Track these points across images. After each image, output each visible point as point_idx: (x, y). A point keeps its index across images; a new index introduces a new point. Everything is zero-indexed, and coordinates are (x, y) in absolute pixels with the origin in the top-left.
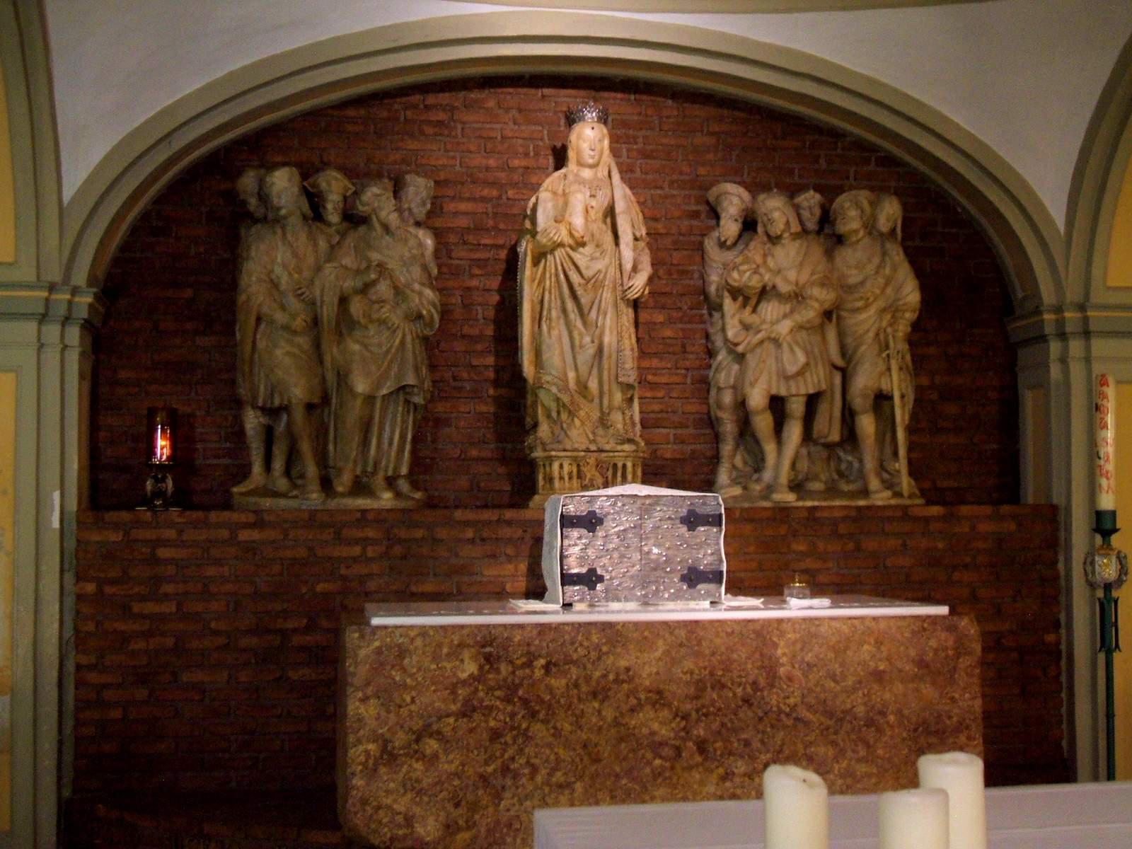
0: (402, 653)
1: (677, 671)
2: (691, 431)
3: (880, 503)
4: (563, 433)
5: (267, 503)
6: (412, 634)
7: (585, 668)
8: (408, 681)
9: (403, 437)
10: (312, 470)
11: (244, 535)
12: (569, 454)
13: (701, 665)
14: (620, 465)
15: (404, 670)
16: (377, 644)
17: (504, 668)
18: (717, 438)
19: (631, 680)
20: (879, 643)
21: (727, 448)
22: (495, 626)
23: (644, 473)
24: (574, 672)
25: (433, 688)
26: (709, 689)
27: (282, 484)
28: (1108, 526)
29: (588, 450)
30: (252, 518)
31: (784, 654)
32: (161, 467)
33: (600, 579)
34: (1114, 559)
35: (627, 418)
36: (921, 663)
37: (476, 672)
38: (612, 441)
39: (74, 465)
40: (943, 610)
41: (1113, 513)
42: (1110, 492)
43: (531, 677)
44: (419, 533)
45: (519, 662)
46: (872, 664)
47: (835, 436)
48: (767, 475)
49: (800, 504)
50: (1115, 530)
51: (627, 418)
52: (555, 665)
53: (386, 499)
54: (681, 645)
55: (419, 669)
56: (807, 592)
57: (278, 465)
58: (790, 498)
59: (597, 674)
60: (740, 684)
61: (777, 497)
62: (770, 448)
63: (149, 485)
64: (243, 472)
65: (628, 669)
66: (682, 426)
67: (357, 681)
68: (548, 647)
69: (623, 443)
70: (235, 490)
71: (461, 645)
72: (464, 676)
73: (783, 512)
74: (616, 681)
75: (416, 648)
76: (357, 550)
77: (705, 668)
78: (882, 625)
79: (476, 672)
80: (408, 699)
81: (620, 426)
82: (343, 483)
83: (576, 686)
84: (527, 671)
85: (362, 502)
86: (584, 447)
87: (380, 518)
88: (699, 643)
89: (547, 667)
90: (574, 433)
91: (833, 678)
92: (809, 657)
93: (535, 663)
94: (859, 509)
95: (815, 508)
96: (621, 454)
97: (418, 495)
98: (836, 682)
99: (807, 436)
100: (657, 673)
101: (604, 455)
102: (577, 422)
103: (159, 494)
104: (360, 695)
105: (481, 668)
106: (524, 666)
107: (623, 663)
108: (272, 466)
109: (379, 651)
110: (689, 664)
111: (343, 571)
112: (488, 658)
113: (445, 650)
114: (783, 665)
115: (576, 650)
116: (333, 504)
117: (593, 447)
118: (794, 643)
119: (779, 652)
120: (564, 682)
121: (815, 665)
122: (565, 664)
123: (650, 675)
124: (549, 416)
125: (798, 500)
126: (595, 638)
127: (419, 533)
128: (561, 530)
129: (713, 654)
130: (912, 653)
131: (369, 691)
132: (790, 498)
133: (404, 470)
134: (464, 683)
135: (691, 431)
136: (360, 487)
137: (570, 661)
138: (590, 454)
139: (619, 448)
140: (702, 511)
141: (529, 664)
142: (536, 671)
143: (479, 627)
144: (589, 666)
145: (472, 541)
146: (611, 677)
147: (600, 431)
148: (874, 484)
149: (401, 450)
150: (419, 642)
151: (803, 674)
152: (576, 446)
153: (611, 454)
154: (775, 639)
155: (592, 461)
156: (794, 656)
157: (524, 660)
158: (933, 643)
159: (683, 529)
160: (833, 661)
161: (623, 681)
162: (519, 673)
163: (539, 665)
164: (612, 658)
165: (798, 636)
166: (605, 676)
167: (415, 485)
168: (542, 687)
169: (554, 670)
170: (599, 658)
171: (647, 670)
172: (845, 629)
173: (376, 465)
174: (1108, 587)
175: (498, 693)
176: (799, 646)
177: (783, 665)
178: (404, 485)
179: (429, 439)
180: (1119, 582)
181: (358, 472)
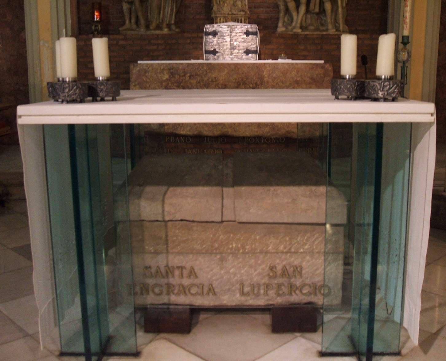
0: (146, 72)
1: (231, 79)
2: (271, 9)
3: (331, 33)
4: (221, 9)
5: (129, 32)
6: (149, 66)
7: (202, 77)
8: (148, 80)
9: (172, 10)
10: (142, 21)
11: (121, 42)
12: (222, 15)
13: (239, 77)
14: (240, 19)
15: (146, 77)
16: (138, 69)
17: (177, 77)
18: (278, 12)
19: (216, 81)
20: (298, 72)
21: (282, 14)
22: (174, 64)
23: (248, 22)
24: (199, 78)
25: (155, 82)
26: (241, 85)
27: (134, 26)
28: (406, 41)
29: (228, 14)
30: (123, 37)
31: (266, 74)
32: (97, 21)
33: (217, 52)
34: (406, 53)
35: (243, 4)
36: (312, 78)
37: (168, 78)
38: (237, 11)
39: (69, 22)
40: (322, 62)
41: (408, 37)
42: (407, 29)
43: (185, 80)
44: (174, 41)
45: (181, 75)
46: (296, 78)
47: (317, 10)
48: (294, 24)
49: (303, 33)
50: (408, 43)
51: (243, 4)
52: (193, 76)
53: (166, 31)
54: (233, 70)
55: (151, 76)
56: (286, 57)
57: (133, 20)
58: (299, 31)
59: (206, 79)
60: (251, 84)
61: (295, 30)
62: (294, 14)
63: (93, 27)
64: (124, 24)
65: (215, 78)
66: (268, 7)
67: (132, 80)
68: (190, 70)
69: (240, 11)
70: (120, 29)
71: (163, 69)
72: (165, 79)
73: (296, 35)
74: (212, 81)
75: (150, 70)
76: (155, 47)
77: (240, 78)
78: (299, 66)
79: (168, 78)
80: (148, 86)
81: (240, 6)
82: (153, 25)
83: (199, 82)
84: (184, 78)
85: (158, 32)
86: (227, 13)
87: (163, 36)
88: (238, 70)
89: (190, 77)
90: (225, 9)
91: (282, 82)
92: (274, 75)
93: (186, 75)
94: (322, 35)
95: (307, 34)
96: (240, 15)
97: (177, 30)
98: (283, 83)
99: (308, 11)
100: (225, 79)
101: (234, 16)
102: (226, 5)
103: (96, 30)
104: (134, 84)
105: (169, 77)
106: (182, 76)
107: (214, 76)
108: (131, 21)
109: (139, 71)
110: (235, 76)
111: (151, 54)
112: (172, 73)
113: (159, 71)
114: (265, 78)
115: (199, 71)
116: (149, 33)
117: (230, 13)
118: (269, 71)
119: (264, 73)
120: (195, 81)
121: (276, 78)
122: (196, 76)
123: (222, 80)
124: (217, 3)
125: (302, 32)
126: (205, 68)
127: (174, 41)
128: (205, 36)
129: (243, 73)
130: (309, 75)
131: (136, 83)
132: (299, 31)
133: (173, 22)
134: (165, 81)
135: (271, 9)
136: (159, 27)
137: (197, 75)
138: (229, 15)
139: (239, 13)
140: (250, 30)
141: (184, 76)
142: (187, 78)
143: (169, 64)
144: (203, 77)
145: (190, 43)
146: (210, 80)
147: (233, 7)
148: (330, 27)
149: (171, 14)
150: (151, 68)
151: (272, 81)
152: (225, 13)
153: (236, 15)
154: (263, 69)
155: (230, 18)
156: (269, 75)
157: (183, 74)
158: (317, 72)
159: (245, 36)
160: (282, 77)
161: (214, 82)
162: (181, 78)
163: (188, 76)
164: (210, 74)
165: (271, 68)
166: (208, 80)
167: (178, 27)
168: (189, 83)
169: (192, 77)
170: (206, 74)
171: (221, 78)
172: (287, 67)
173: (162, 21)
174: (404, 62)
175: (175, 84)
176: (271, 72)
177: (265, 78)
178: (173, 27)
179: (183, 12)
180: (407, 60)
181: (158, 23)
